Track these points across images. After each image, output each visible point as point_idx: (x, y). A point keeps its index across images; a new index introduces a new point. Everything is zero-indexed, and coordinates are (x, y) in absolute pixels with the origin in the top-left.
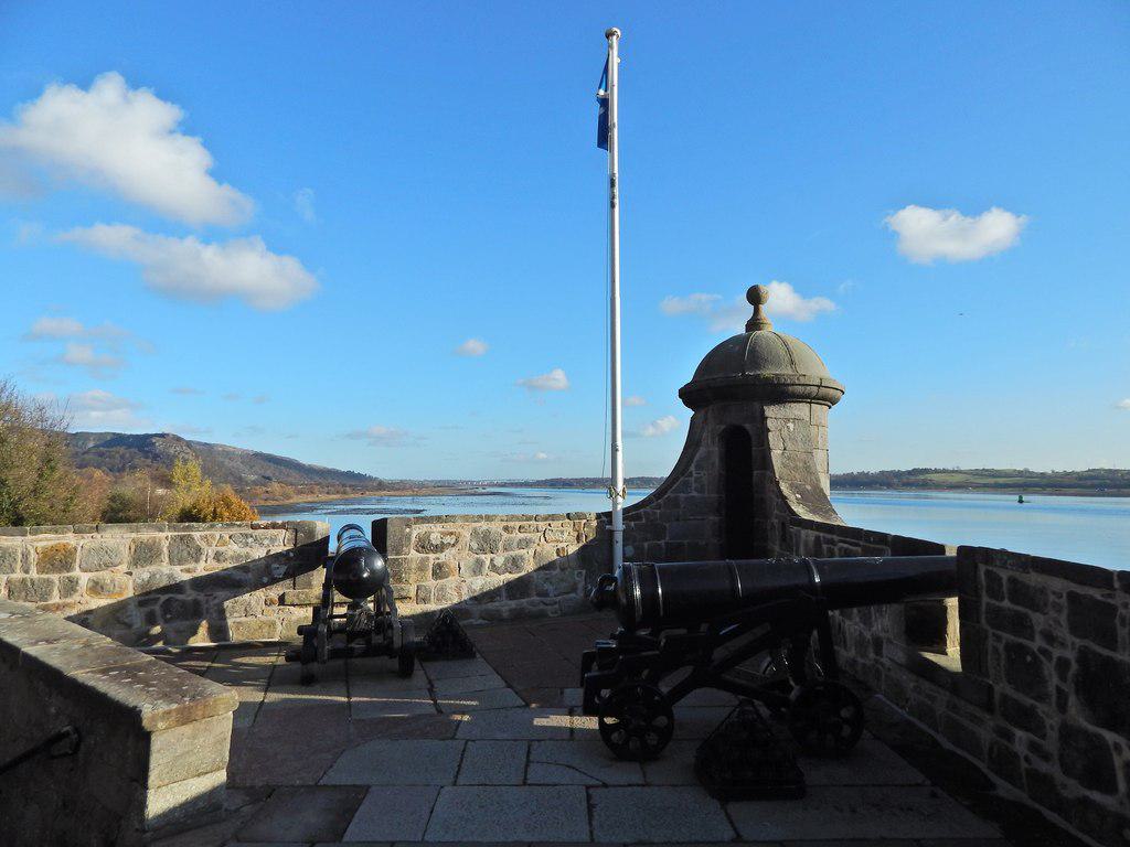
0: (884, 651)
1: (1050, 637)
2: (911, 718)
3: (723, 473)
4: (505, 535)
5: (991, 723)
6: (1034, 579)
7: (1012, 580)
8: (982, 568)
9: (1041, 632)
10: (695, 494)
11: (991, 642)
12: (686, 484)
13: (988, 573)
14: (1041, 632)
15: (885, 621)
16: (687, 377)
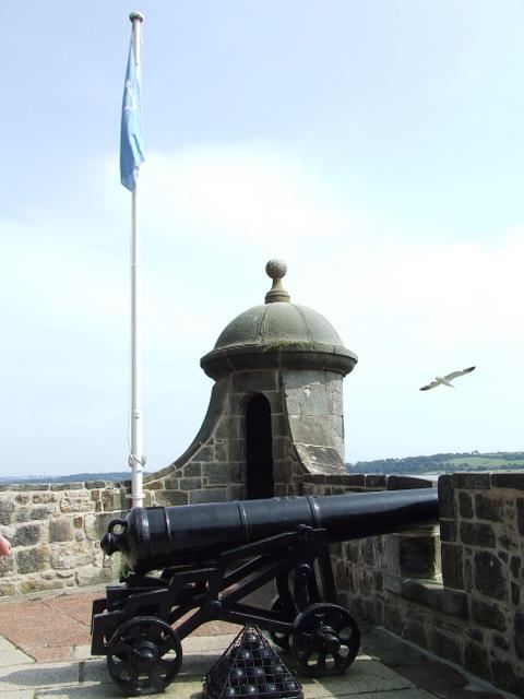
0: (384, 586)
1: (506, 542)
2: (406, 642)
3: (244, 439)
4: (18, 506)
5: (467, 629)
6: (494, 493)
7: (479, 498)
8: (457, 492)
9: (500, 539)
10: (215, 461)
11: (464, 557)
12: (207, 452)
13: (461, 495)
14: (500, 539)
15: (384, 552)
16: (208, 346)
